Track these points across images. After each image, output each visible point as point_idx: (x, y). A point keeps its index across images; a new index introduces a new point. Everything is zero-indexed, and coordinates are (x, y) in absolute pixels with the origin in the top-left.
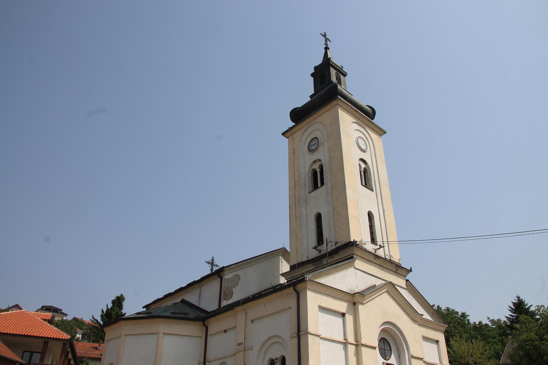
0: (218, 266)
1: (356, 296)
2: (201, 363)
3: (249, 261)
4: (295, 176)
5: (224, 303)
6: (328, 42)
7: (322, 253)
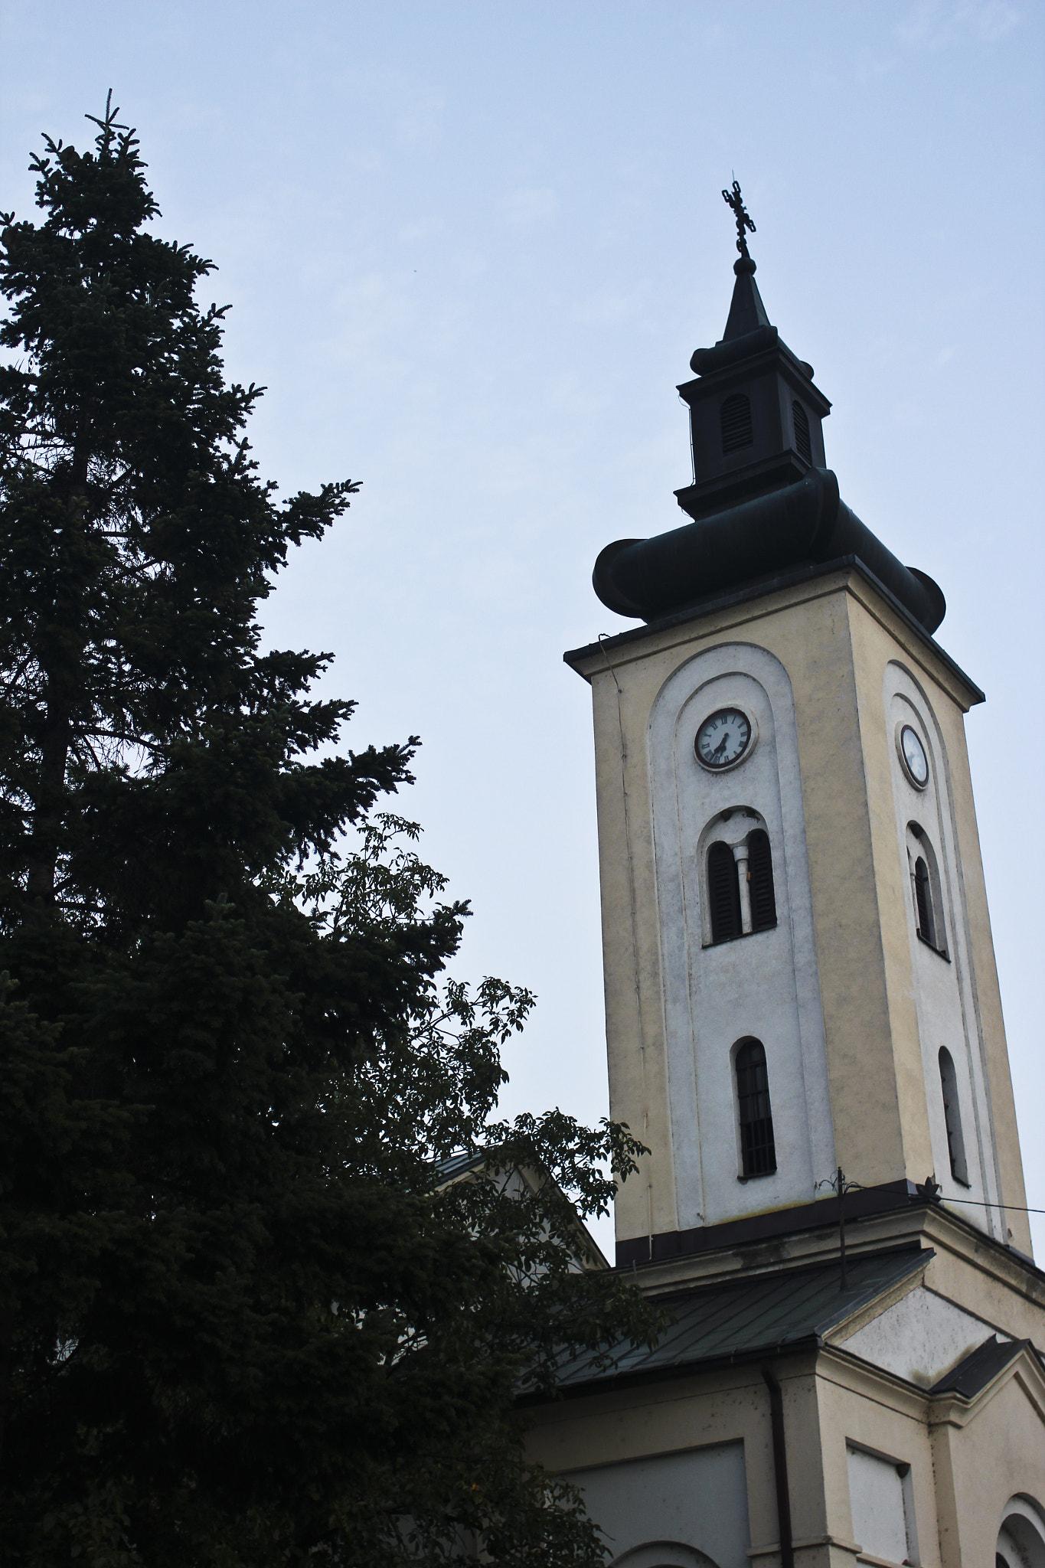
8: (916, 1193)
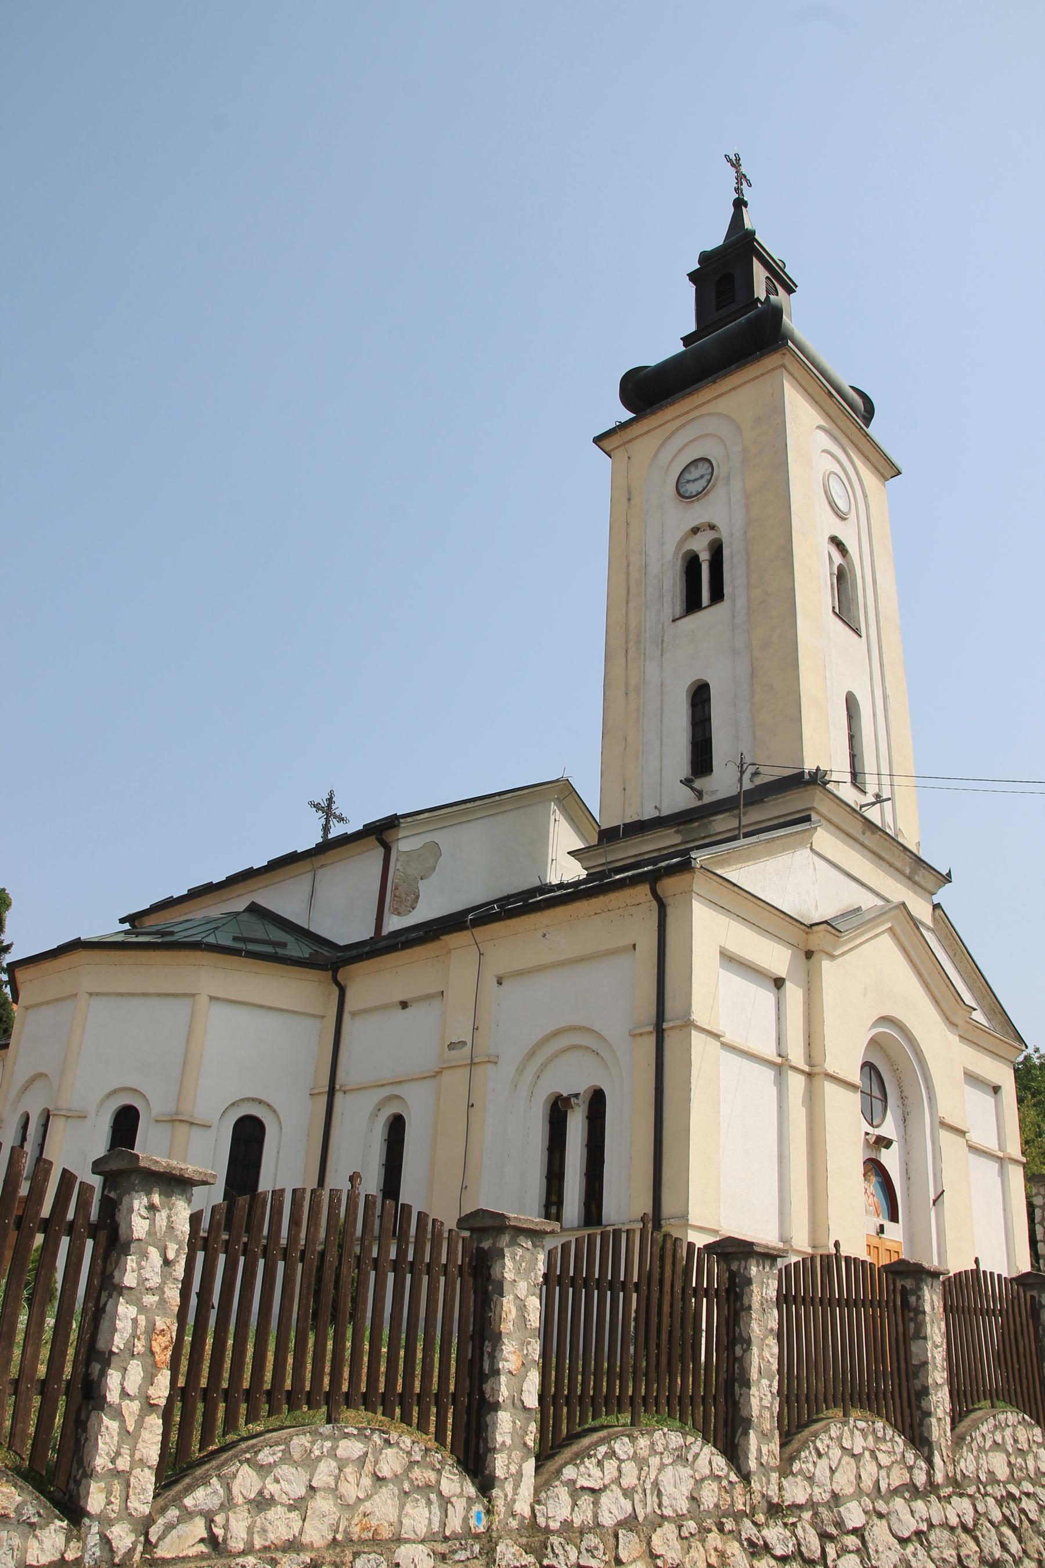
0: (343, 819)
1: (817, 932)
2: (320, 1093)
3: (469, 805)
4: (628, 566)
5: (394, 923)
6: (745, 185)
7: (707, 799)
8: (809, 777)
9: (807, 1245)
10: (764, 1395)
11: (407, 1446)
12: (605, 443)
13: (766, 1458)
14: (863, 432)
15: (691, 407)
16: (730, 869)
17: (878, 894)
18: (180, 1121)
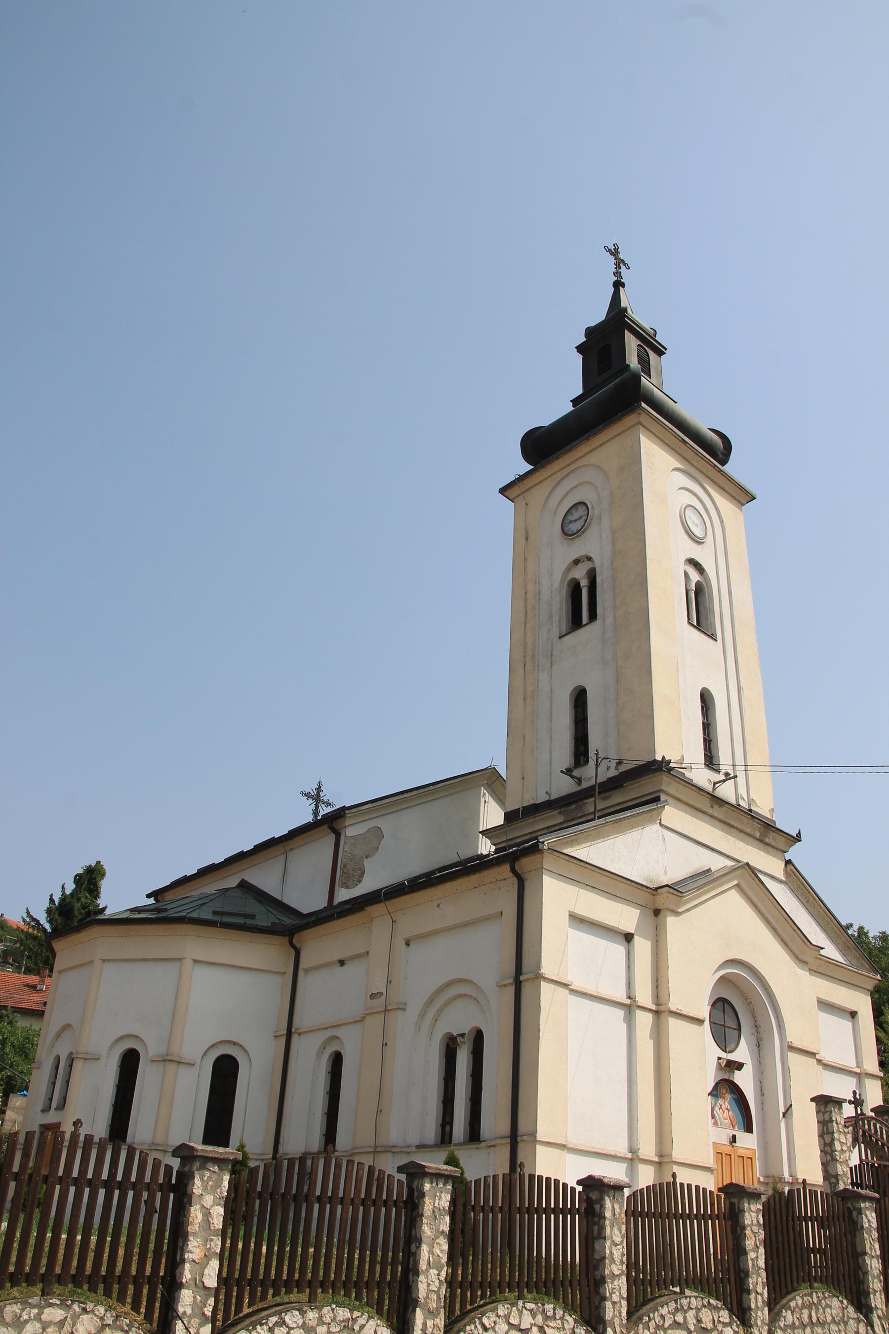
1: (661, 893)
2: (281, 1036)
3: (406, 795)
4: (526, 593)
5: (343, 895)
7: (585, 785)
9: (654, 1155)
10: (432, 1281)
11: (101, 1313)
12: (507, 493)
13: (431, 1330)
14: (717, 468)
15: (572, 461)
16: (580, 847)
17: (728, 857)
18: (170, 1060)
